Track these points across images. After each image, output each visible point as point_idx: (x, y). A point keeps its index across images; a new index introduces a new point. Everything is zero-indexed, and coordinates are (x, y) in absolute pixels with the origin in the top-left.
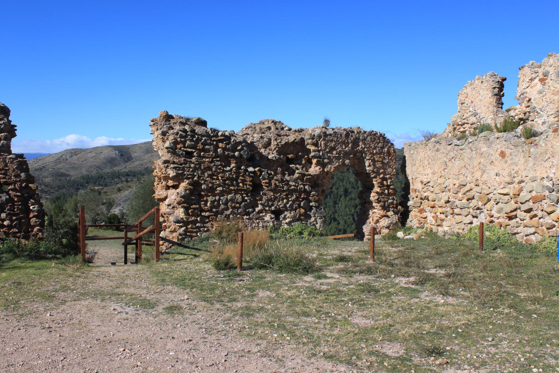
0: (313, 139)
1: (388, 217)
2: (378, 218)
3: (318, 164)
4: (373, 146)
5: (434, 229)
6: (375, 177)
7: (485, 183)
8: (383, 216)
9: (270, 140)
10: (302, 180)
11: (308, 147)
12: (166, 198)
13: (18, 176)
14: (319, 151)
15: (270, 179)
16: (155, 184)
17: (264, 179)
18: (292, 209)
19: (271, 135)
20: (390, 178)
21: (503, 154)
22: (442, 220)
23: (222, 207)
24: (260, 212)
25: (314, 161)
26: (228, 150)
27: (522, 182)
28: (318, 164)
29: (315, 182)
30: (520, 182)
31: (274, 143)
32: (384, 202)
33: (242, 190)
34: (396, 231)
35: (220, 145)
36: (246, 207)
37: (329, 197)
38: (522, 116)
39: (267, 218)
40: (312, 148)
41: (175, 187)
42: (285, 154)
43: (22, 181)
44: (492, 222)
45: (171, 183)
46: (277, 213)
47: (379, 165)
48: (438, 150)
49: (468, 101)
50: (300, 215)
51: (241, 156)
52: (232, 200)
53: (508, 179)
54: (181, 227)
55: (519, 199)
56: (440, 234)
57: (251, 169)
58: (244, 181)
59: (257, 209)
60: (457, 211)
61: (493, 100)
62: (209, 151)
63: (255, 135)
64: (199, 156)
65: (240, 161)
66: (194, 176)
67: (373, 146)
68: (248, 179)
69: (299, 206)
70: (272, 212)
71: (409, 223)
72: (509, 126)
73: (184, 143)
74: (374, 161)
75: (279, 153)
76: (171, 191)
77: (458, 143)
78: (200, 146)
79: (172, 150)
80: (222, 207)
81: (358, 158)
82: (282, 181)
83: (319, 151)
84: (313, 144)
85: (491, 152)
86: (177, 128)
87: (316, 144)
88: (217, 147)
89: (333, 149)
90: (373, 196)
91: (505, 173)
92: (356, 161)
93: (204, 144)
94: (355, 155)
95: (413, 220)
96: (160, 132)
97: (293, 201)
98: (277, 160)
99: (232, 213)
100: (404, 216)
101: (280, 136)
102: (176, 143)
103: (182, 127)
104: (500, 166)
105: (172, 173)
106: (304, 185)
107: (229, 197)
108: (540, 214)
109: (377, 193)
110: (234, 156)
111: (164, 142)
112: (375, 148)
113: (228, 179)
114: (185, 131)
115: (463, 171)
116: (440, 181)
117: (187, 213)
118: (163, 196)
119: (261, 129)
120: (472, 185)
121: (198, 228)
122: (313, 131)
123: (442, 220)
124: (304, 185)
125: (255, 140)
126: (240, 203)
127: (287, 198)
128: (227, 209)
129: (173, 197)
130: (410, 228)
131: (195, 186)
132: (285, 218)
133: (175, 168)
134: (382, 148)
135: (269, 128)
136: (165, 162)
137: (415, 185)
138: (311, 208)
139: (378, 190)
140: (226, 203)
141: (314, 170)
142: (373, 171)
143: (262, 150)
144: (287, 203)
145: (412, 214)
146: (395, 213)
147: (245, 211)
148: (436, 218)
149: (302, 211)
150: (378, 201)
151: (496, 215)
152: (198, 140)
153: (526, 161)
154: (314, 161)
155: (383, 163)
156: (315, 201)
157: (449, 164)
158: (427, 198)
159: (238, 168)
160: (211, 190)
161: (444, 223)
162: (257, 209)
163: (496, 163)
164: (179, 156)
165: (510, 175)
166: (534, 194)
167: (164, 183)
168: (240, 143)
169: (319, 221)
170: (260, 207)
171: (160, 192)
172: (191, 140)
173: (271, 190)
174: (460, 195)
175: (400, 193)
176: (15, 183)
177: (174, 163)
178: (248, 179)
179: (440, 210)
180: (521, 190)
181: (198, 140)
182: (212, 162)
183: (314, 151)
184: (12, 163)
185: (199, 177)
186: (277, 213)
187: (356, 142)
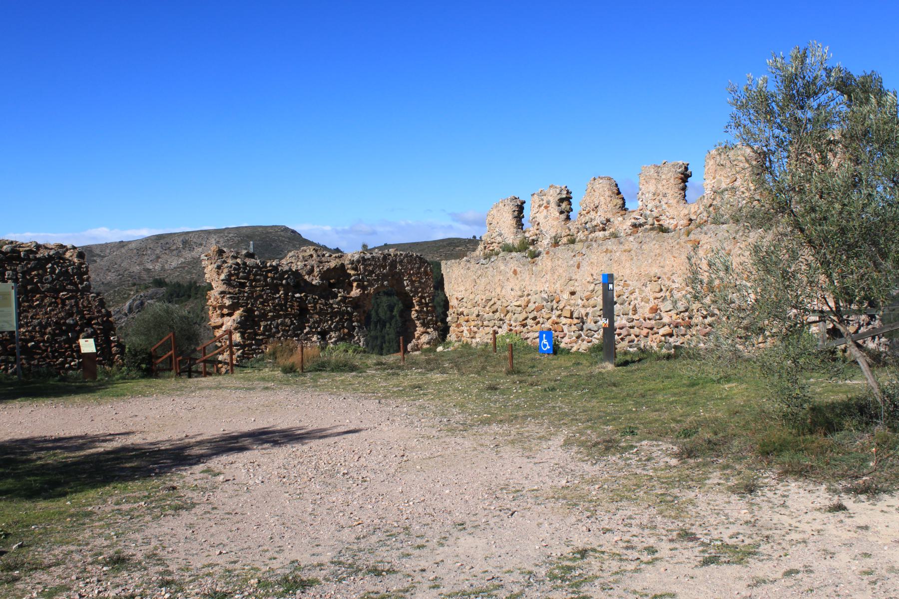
0: (352, 264)
1: (428, 333)
2: (423, 337)
3: (358, 287)
4: (409, 267)
5: (469, 340)
6: (414, 296)
7: (504, 297)
8: (423, 333)
9: (313, 267)
10: (344, 303)
11: (348, 271)
12: (222, 324)
13: (100, 311)
14: (359, 275)
15: (315, 303)
16: (210, 312)
17: (310, 303)
18: (336, 329)
19: (313, 262)
20: (428, 296)
21: (515, 272)
22: (475, 333)
23: (274, 330)
24: (307, 333)
25: (355, 284)
26: (276, 279)
27: (528, 295)
28: (358, 287)
29: (356, 303)
30: (528, 295)
31: (316, 270)
32: (424, 319)
33: (290, 314)
34: (436, 346)
35: (269, 275)
36: (295, 329)
37: (388, 325)
38: (534, 237)
39: (315, 338)
40: (352, 272)
41: (230, 315)
42: (328, 280)
43: (103, 316)
44: (511, 330)
45: (225, 311)
46: (323, 335)
47: (417, 284)
48: (469, 269)
49: (495, 222)
50: (344, 335)
51: (288, 283)
52: (282, 324)
53: (520, 293)
54: (238, 350)
55: (528, 309)
56: (474, 345)
57: (297, 295)
58: (292, 307)
59: (305, 331)
60: (485, 323)
61: (514, 222)
62: (259, 280)
63: (299, 263)
64: (251, 285)
65: (287, 288)
66: (248, 304)
67: (409, 267)
68: (296, 304)
69: (343, 327)
70: (319, 333)
71: (448, 338)
72: (524, 246)
73: (237, 275)
74: (412, 282)
75: (322, 278)
76: (226, 319)
77: (484, 262)
78: (252, 277)
79: (228, 281)
80: (274, 330)
81: (397, 278)
82: (326, 304)
83: (359, 275)
84: (353, 269)
85: (507, 270)
86: (230, 262)
87: (355, 269)
88: (266, 277)
89: (372, 272)
90: (414, 315)
91: (517, 288)
92: (395, 282)
93: (255, 275)
94: (393, 276)
95: (452, 337)
96: (215, 266)
97: (337, 322)
98: (321, 285)
99: (283, 336)
100: (444, 331)
101: (321, 262)
102: (230, 275)
103: (234, 261)
104: (513, 283)
105: (228, 302)
106: (347, 307)
107: (279, 321)
108: (541, 320)
109: (416, 311)
110: (281, 284)
111: (219, 274)
112: (412, 269)
113: (278, 305)
114: (237, 264)
115: (488, 288)
116: (472, 297)
117: (243, 336)
118: (220, 323)
119: (303, 257)
120: (496, 299)
121: (254, 350)
122: (353, 256)
123: (475, 333)
124: (347, 307)
125: (299, 267)
126: (289, 326)
127: (332, 320)
128: (279, 332)
129: (229, 324)
130: (450, 342)
131: (249, 312)
132: (330, 338)
133: (230, 298)
134: (419, 268)
135: (311, 256)
136: (222, 293)
137: (453, 302)
138: (354, 328)
139: (417, 308)
140: (277, 327)
141: (355, 292)
142: (411, 291)
143: (306, 277)
144: (332, 324)
145: (451, 329)
146: (435, 330)
147: (294, 333)
148: (470, 331)
149: (346, 331)
150: (418, 318)
151: (514, 324)
152: (250, 271)
153: (531, 278)
154: (355, 284)
155: (420, 282)
156: (357, 321)
157: (478, 281)
158: (462, 313)
159: (286, 294)
160: (264, 316)
161: (477, 335)
162: (305, 331)
163: (511, 280)
164: (234, 287)
165: (520, 290)
166: (537, 304)
167: (219, 312)
168: (286, 272)
169: (362, 339)
170: (307, 329)
171: (215, 320)
172: (244, 272)
173: (317, 313)
174: (487, 308)
175: (440, 310)
176: (97, 318)
177: (230, 293)
178: (296, 304)
179: (473, 323)
180: (529, 302)
181: (250, 271)
182: (263, 290)
183: (354, 275)
184: (94, 300)
185: (252, 305)
186: (323, 335)
187: (393, 265)
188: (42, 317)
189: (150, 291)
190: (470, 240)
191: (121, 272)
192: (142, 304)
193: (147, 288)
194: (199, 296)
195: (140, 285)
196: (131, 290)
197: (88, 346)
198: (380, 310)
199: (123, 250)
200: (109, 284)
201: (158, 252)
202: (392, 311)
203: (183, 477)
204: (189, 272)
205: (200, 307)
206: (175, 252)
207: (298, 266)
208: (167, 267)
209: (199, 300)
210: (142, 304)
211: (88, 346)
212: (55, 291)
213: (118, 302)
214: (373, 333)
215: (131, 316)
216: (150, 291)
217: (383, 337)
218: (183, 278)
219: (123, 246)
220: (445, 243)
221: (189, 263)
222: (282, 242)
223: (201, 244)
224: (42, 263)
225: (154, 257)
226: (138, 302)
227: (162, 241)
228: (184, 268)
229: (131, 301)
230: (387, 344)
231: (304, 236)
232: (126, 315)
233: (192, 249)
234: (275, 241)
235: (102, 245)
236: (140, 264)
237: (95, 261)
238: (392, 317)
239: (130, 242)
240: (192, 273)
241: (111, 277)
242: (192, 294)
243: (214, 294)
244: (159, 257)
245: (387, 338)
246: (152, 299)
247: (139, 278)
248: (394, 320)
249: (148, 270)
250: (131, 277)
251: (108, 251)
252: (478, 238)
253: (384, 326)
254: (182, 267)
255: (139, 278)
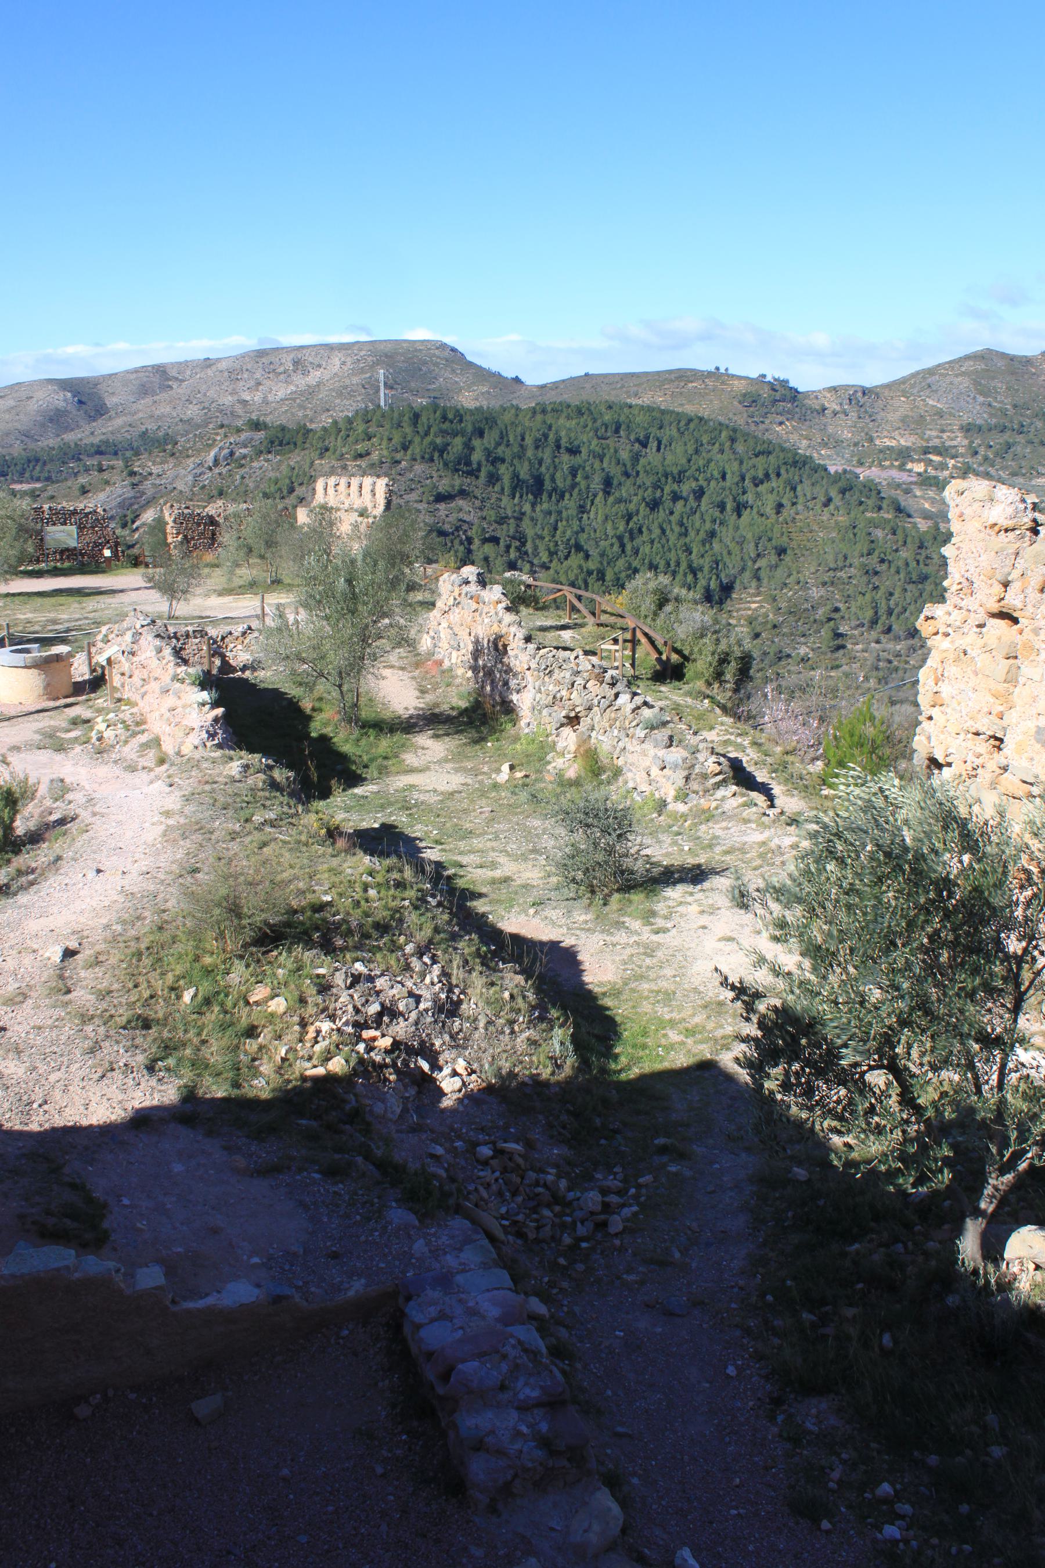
65: (205, 524)
79: (175, 521)
131: (185, 537)
188: (88, 540)
189: (244, 436)
190: (709, 373)
191: (207, 405)
192: (232, 454)
193: (239, 431)
194: (307, 445)
195: (229, 426)
196: (217, 434)
197: (107, 553)
198: (558, 475)
199: (210, 372)
200: (189, 421)
201: (258, 375)
202: (574, 476)
203: (666, 899)
204: (302, 407)
205: (308, 461)
206: (282, 377)
207: (212, 512)
208: (270, 398)
209: (307, 452)
210: (232, 454)
211: (107, 553)
212: (93, 528)
213: (199, 451)
214: (545, 506)
215: (217, 471)
216: (244, 436)
217: (560, 513)
218: (293, 414)
219: (210, 366)
220: (673, 376)
221: (302, 393)
222: (437, 364)
223: (319, 366)
224: (87, 515)
225: (252, 383)
226: (226, 451)
227: (264, 360)
228: (294, 400)
229: (217, 449)
230: (564, 523)
231: (469, 358)
232: (210, 469)
233: (306, 373)
234: (425, 363)
235: (180, 363)
236: (234, 393)
237: (171, 387)
238: (574, 485)
239: (219, 360)
240: (305, 409)
241: (192, 411)
242: (299, 443)
243: (169, 527)
244: (259, 384)
245: (564, 514)
246: (246, 447)
247: (232, 413)
248: (576, 490)
249: (244, 403)
250: (221, 411)
251: (188, 373)
252: (722, 370)
253: (562, 497)
254: (291, 398)
255: (232, 413)
